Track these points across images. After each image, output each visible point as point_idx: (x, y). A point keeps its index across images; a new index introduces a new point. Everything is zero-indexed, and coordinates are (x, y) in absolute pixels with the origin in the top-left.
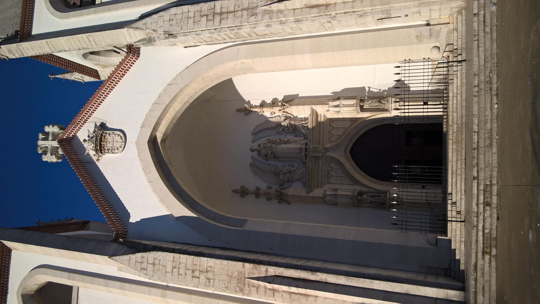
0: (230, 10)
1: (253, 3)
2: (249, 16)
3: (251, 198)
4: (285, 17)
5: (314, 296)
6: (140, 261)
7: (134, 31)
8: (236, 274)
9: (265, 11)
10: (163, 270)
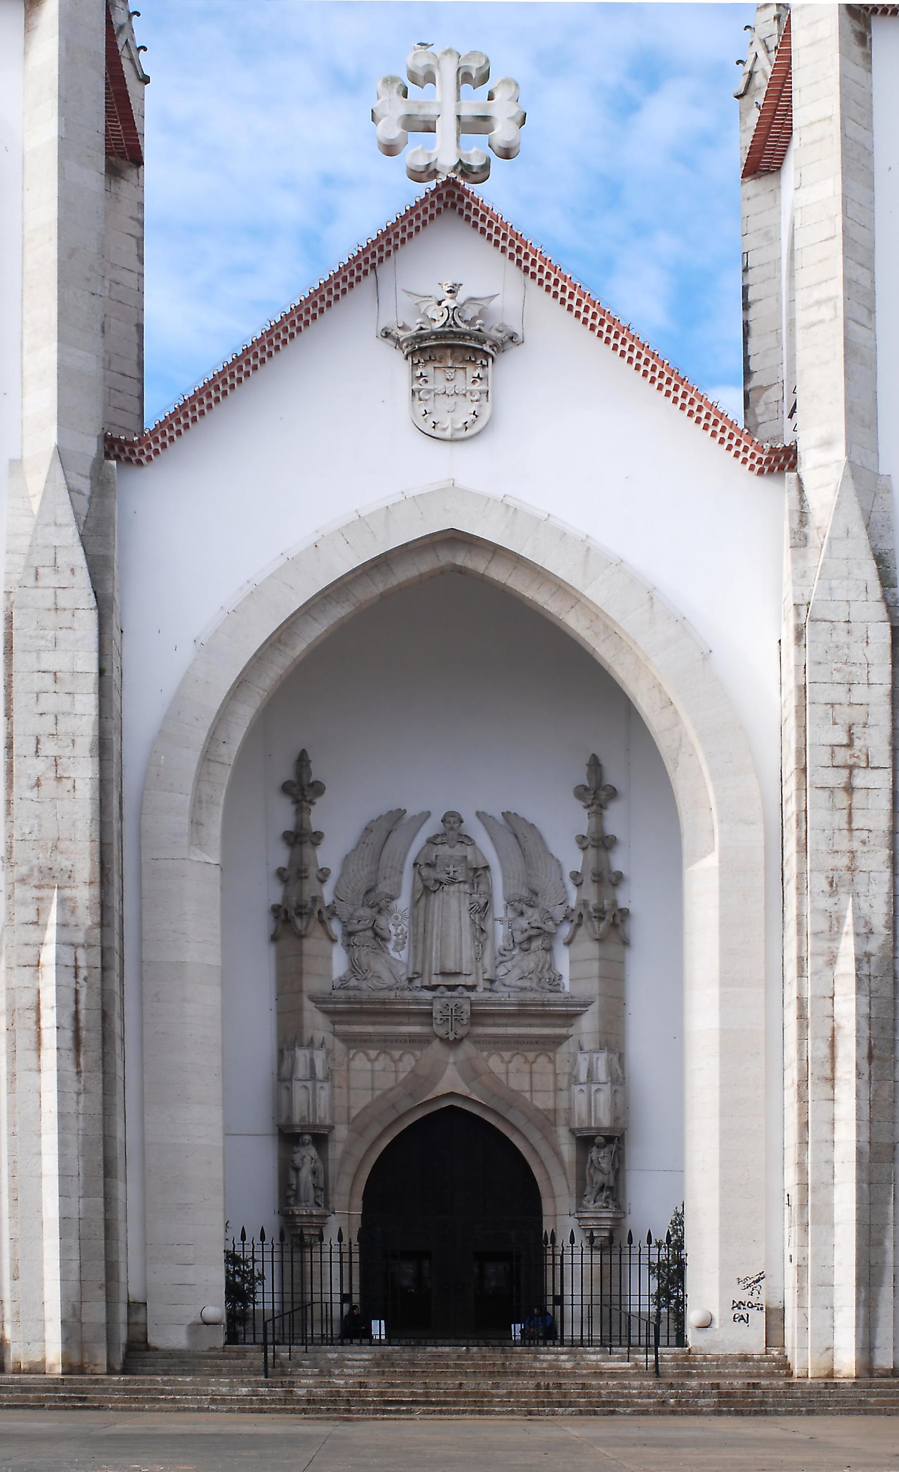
0: (857, 814)
1: (869, 883)
2: (830, 874)
3: (281, 857)
4: (814, 973)
5: (39, 1066)
6: (59, 562)
7: (833, 487)
8: (66, 864)
9: (840, 920)
10: (42, 642)
